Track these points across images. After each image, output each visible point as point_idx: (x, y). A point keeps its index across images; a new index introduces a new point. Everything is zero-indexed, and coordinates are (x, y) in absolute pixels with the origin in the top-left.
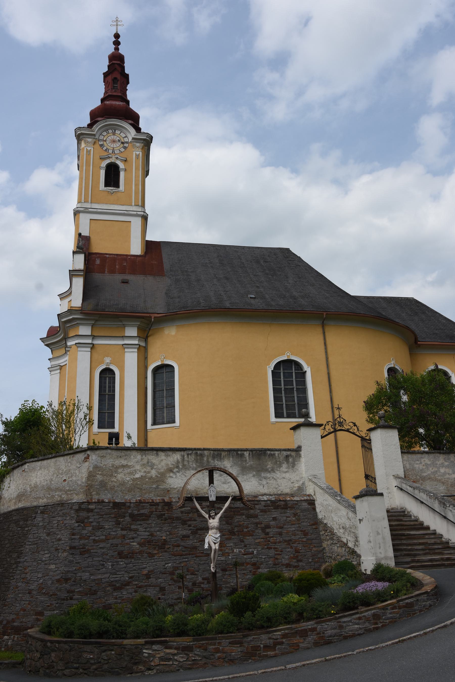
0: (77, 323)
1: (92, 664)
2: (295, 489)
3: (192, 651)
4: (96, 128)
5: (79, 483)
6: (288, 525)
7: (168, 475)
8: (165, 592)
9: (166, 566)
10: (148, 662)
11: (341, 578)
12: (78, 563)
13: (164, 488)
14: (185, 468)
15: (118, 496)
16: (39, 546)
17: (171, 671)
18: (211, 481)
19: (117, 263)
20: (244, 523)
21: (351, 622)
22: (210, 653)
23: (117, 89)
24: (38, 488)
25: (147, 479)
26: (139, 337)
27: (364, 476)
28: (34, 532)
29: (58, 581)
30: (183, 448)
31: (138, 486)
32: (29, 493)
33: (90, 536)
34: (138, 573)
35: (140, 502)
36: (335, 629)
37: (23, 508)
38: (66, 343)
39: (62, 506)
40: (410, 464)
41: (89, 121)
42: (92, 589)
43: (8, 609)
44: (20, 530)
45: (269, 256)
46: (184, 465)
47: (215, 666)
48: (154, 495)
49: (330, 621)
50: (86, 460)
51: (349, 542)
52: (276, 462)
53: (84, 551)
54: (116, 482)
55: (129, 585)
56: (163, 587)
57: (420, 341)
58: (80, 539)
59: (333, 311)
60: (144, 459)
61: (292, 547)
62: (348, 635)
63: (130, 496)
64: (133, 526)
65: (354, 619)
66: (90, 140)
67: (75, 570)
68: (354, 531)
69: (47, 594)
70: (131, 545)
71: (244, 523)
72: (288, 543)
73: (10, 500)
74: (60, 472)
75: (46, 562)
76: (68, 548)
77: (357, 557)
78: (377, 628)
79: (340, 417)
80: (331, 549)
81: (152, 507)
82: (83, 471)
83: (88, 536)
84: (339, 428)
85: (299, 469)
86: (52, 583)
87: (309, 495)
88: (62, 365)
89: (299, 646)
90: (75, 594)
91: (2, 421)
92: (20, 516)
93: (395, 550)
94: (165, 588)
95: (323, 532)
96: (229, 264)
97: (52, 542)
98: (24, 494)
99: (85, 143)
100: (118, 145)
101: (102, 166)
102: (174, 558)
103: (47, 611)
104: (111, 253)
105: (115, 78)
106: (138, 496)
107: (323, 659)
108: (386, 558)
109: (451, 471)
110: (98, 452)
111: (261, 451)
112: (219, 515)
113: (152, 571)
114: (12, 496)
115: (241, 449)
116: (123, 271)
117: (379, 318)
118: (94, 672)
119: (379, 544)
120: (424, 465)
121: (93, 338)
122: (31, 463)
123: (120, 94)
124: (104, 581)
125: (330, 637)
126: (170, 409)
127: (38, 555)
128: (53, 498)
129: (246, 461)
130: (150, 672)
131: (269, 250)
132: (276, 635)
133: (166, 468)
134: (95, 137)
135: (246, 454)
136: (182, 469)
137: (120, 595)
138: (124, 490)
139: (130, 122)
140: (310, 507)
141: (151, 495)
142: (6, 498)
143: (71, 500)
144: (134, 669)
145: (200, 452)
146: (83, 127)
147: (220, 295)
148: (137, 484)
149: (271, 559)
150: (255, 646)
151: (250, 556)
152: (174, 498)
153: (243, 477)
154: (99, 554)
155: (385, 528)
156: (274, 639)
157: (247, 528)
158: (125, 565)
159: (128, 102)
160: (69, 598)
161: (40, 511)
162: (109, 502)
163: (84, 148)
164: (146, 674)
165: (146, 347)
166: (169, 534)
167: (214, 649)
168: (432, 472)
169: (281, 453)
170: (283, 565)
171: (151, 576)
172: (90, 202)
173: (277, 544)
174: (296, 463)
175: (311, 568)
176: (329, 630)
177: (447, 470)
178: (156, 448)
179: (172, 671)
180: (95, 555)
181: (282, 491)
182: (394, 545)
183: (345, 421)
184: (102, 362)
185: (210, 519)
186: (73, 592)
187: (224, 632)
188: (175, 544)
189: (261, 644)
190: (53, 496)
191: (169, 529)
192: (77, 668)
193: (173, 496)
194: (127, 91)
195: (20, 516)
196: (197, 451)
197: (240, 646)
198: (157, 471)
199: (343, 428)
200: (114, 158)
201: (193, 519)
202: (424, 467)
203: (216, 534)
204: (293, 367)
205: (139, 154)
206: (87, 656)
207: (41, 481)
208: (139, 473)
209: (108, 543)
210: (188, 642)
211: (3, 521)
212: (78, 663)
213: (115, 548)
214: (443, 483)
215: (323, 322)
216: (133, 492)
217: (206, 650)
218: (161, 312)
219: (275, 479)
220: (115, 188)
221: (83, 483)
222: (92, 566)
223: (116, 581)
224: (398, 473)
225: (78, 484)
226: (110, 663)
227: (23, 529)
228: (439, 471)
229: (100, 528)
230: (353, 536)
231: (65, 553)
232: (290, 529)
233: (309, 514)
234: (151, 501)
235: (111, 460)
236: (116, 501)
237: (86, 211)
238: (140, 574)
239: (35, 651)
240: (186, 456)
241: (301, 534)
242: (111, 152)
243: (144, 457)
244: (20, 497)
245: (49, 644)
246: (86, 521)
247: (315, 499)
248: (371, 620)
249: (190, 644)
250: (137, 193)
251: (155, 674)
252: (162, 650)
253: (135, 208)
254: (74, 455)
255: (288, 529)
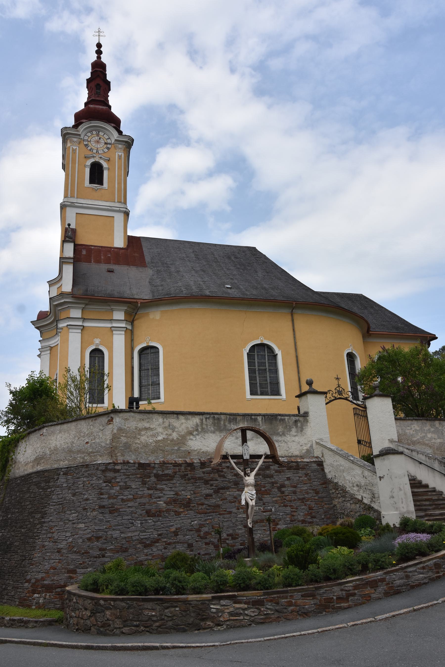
0: (68, 307)
1: (155, 621)
2: (304, 451)
3: (263, 605)
4: (81, 128)
5: (103, 444)
6: (301, 484)
7: (188, 438)
8: (192, 548)
9: (193, 523)
10: (216, 617)
11: (368, 532)
12: (108, 521)
13: (185, 450)
14: (204, 431)
15: (142, 458)
16: (65, 506)
17: (242, 626)
18: (244, 440)
19: (102, 254)
20: (261, 483)
21: (417, 572)
22: (282, 607)
23: (100, 94)
24: (58, 451)
25: (168, 441)
26: (127, 321)
27: (357, 441)
28: (58, 493)
29: (89, 539)
30: (201, 412)
31: (161, 448)
32: (49, 456)
33: (118, 496)
34: (167, 531)
35: (164, 463)
36: (402, 579)
37: (44, 470)
38: (57, 325)
39: (86, 467)
40: (402, 430)
41: (73, 123)
42: (124, 546)
43: (36, 568)
44: (42, 491)
45: (238, 253)
46: (203, 429)
47: (289, 620)
48: (176, 456)
49: (397, 571)
50: (109, 423)
51: (364, 498)
52: (286, 426)
53: (113, 510)
54: (139, 444)
55: (158, 542)
56: (190, 544)
57: (371, 331)
58: (109, 498)
59: (301, 301)
60: (165, 422)
61: (305, 505)
62: (415, 584)
63: (153, 457)
64: (159, 485)
65: (419, 569)
66: (75, 140)
67: (106, 528)
68: (370, 488)
69: (78, 552)
70: (158, 504)
71: (261, 483)
72: (302, 501)
73: (27, 464)
74: (82, 434)
75: (74, 521)
76: (97, 507)
77: (375, 512)
78: (439, 577)
79: (339, 386)
80: (344, 506)
81: (175, 467)
82: (107, 433)
83: (116, 496)
84: (339, 396)
85: (307, 433)
86: (83, 541)
87: (317, 457)
88: (52, 346)
89: (370, 597)
90: (106, 551)
91: (10, 390)
92: (41, 478)
93: (415, 505)
94: (192, 544)
95: (334, 491)
96: (204, 258)
97: (78, 502)
98: (43, 457)
99: (71, 142)
100: (101, 146)
101: (87, 164)
102: (199, 516)
103: (80, 569)
104: (96, 245)
105: (98, 85)
106: (161, 457)
107: (412, 608)
108: (408, 512)
109: (436, 436)
110: (121, 415)
111: (273, 416)
112: (254, 473)
113: (179, 528)
114: (29, 460)
115: (254, 414)
116: (108, 261)
117: (339, 308)
118: (157, 629)
119: (402, 499)
120: (413, 431)
121: (83, 321)
122: (50, 427)
123: (102, 99)
124: (134, 538)
125: (398, 587)
126: (155, 386)
127: (64, 515)
128: (75, 460)
129: (259, 425)
130: (219, 628)
131: (238, 248)
132: (349, 586)
133: (186, 431)
134: (80, 137)
135: (259, 418)
136: (201, 431)
137: (150, 552)
138: (147, 452)
139: (113, 125)
140: (319, 467)
141: (173, 456)
142: (21, 462)
143: (95, 461)
144: (202, 625)
145: (218, 416)
146: (69, 127)
147: (200, 285)
148: (159, 446)
149: (288, 516)
150: (328, 598)
151: (268, 513)
152: (195, 459)
153: (257, 440)
154: (128, 512)
155: (406, 484)
156: (346, 590)
157: (264, 488)
158: (153, 523)
159: (110, 107)
160: (101, 556)
161: (63, 473)
162: (134, 463)
163: (70, 147)
164: (216, 629)
165: (133, 330)
166: (193, 493)
167: (286, 602)
168: (420, 437)
169: (290, 418)
170: (299, 521)
171: (179, 533)
172: (76, 197)
173: (292, 502)
174: (304, 427)
175: (324, 524)
176: (397, 580)
177: (433, 435)
178: (177, 411)
179: (243, 626)
180: (124, 514)
181: (292, 454)
182: (414, 501)
183: (344, 390)
184: (92, 343)
185: (246, 477)
186: (104, 549)
187: (293, 585)
188: (199, 502)
189: (333, 596)
190: (75, 459)
191: (192, 489)
192: (137, 626)
193: (193, 457)
194: (109, 98)
195: (41, 478)
196: (214, 415)
197: (313, 599)
198: (178, 434)
199: (342, 397)
200: (97, 157)
201: (214, 479)
202: (414, 433)
203: (252, 490)
204: (266, 350)
205: (121, 155)
206: (148, 613)
207: (61, 444)
208: (162, 435)
209: (136, 502)
210: (258, 596)
211: (22, 484)
212: (138, 621)
213: (143, 507)
214: (430, 447)
215: (292, 311)
216: (156, 453)
217: (277, 603)
218: (147, 298)
219: (286, 442)
220: (99, 186)
221: (107, 444)
222: (121, 524)
223: (146, 538)
224: (393, 438)
225: (102, 445)
226: (175, 619)
227: (45, 490)
228: (427, 435)
229: (127, 487)
230: (370, 493)
231: (94, 512)
232: (303, 488)
233: (318, 474)
234: (174, 462)
235: (135, 423)
236: (141, 462)
237: (73, 205)
238: (168, 532)
239: (83, 609)
240: (204, 420)
241: (313, 492)
242: (95, 152)
243: (165, 420)
244: (38, 460)
245: (102, 602)
246: (113, 481)
247: (323, 460)
248: (433, 569)
249: (260, 598)
250: (119, 190)
251: (225, 629)
252: (231, 605)
253: (117, 205)
254: (96, 418)
255: (301, 488)
